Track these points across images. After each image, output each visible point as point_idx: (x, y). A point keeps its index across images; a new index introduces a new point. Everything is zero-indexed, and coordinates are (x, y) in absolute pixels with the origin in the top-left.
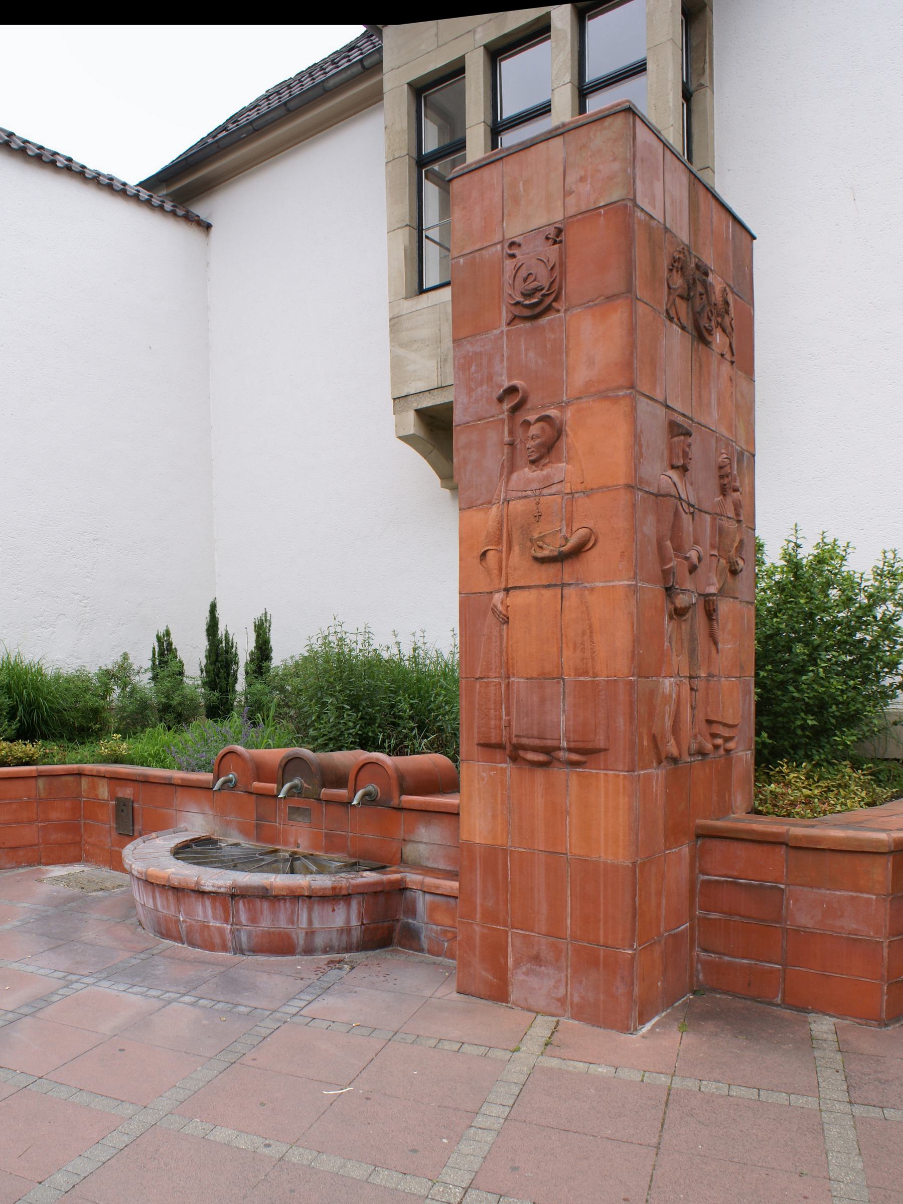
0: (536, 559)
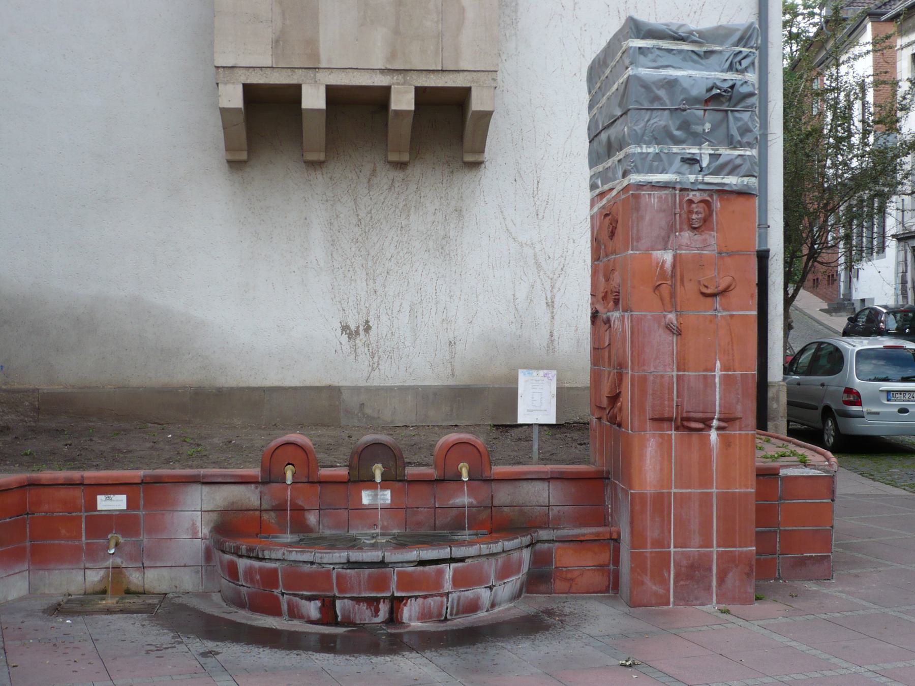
0: (705, 295)
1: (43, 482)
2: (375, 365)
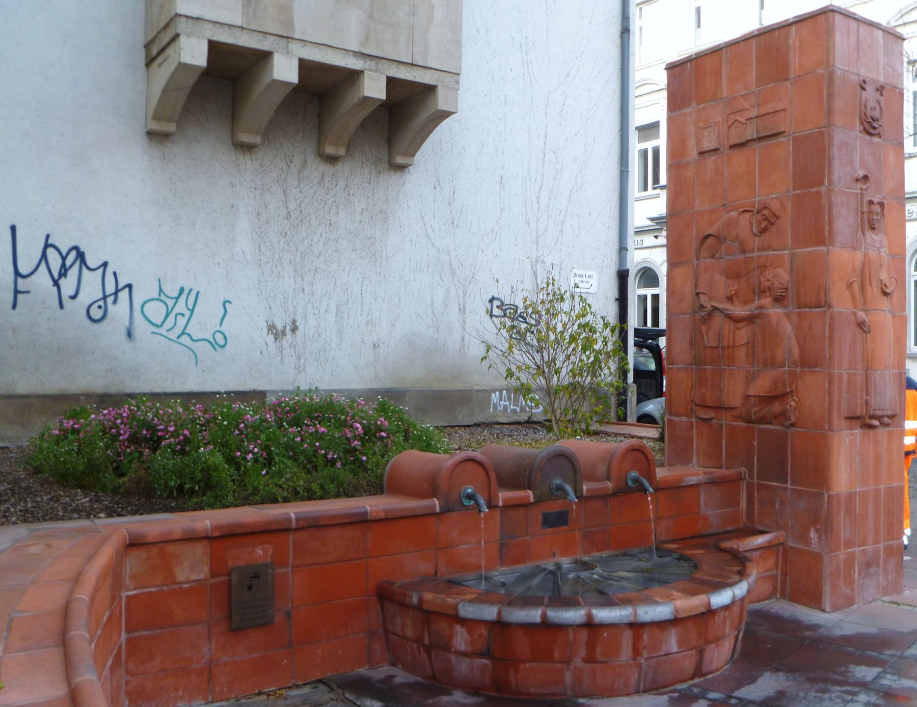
2: (302, 368)
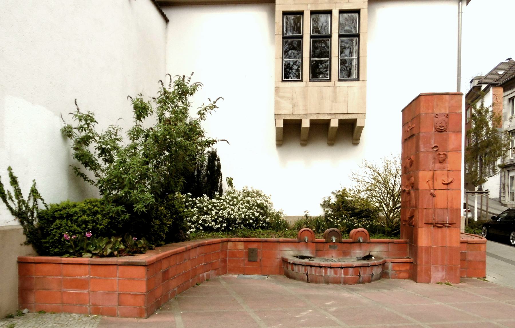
0: (443, 184)
1: (30, 261)
